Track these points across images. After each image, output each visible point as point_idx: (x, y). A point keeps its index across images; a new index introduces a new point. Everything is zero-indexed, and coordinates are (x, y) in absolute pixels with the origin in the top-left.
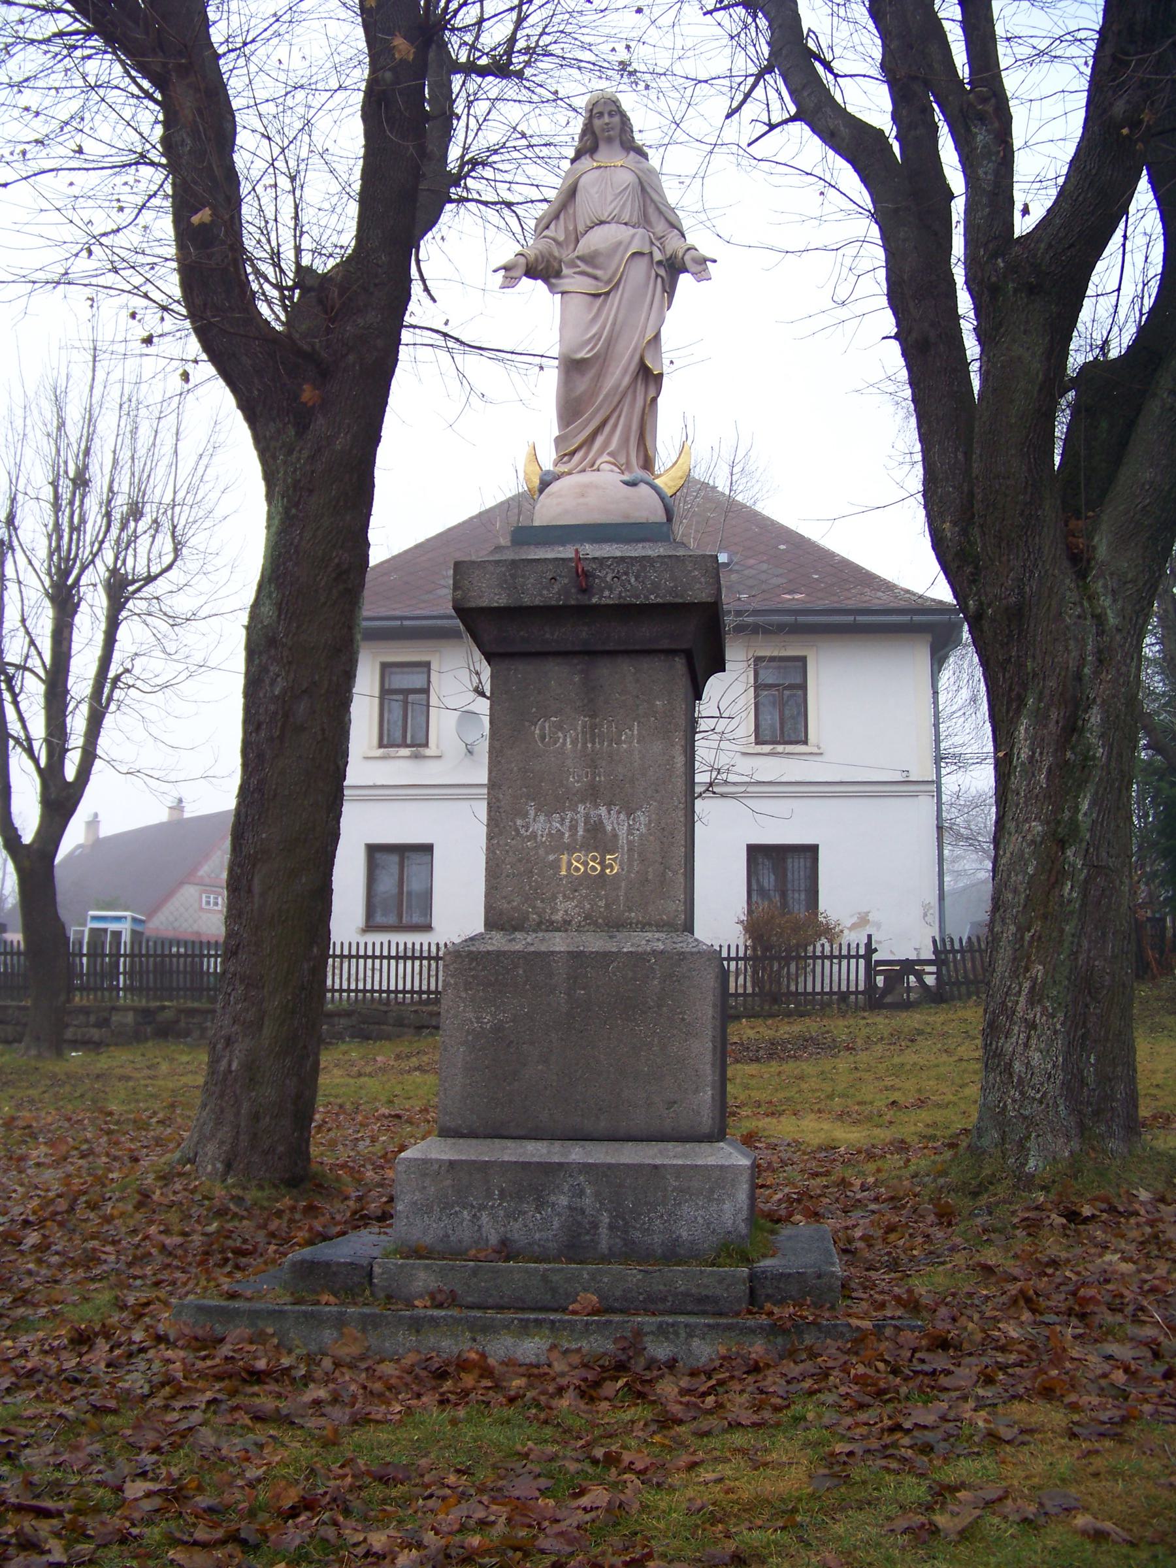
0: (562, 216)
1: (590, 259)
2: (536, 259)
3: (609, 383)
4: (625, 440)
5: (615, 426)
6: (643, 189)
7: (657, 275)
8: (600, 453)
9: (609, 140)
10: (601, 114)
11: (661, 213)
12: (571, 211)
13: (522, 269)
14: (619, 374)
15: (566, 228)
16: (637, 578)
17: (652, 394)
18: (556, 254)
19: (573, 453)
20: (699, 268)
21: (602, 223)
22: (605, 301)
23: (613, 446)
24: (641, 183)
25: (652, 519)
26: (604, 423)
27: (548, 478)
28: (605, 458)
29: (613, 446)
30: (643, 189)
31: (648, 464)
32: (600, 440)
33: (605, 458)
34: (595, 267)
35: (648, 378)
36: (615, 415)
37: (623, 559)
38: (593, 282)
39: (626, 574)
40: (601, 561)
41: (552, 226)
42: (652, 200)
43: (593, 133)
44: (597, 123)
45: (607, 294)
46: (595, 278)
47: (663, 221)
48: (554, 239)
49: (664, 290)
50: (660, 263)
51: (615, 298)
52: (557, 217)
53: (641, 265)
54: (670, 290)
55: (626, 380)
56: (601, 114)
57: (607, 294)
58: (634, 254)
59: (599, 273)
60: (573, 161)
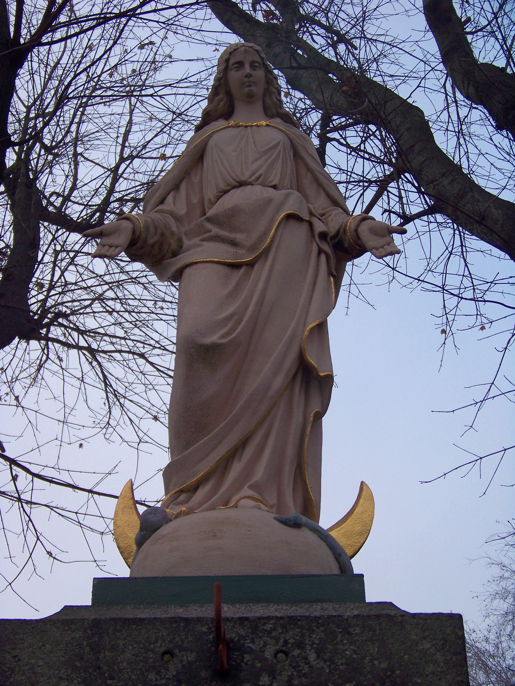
0: (183, 187)
1: (227, 220)
2: (147, 227)
3: (252, 385)
4: (276, 472)
5: (261, 450)
6: (296, 154)
7: (320, 251)
8: (237, 486)
9: (250, 98)
10: (240, 64)
11: (320, 185)
12: (196, 180)
13: (123, 239)
14: (268, 370)
15: (189, 203)
16: (319, 652)
17: (316, 408)
18: (174, 229)
19: (195, 488)
20: (382, 241)
21: (241, 184)
22: (247, 275)
23: (259, 473)
24: (293, 146)
25: (328, 572)
26: (244, 443)
27: (154, 518)
28: (246, 491)
29: (259, 473)
30: (296, 154)
31: (310, 506)
32: (236, 468)
33: (246, 491)
34: (233, 229)
35: (313, 381)
36: (261, 433)
37: (293, 620)
38: (231, 249)
39: (300, 645)
40: (255, 625)
41: (170, 199)
42: (309, 169)
43: (229, 94)
44: (234, 76)
45: (251, 264)
46: (234, 243)
47: (323, 195)
48: (171, 213)
49: (330, 274)
50: (323, 236)
51: (262, 271)
52: (176, 187)
53: (297, 234)
54: (336, 275)
55: (279, 382)
56: (240, 64)
57: (251, 264)
58: (290, 217)
59: (239, 237)
60: (198, 128)
